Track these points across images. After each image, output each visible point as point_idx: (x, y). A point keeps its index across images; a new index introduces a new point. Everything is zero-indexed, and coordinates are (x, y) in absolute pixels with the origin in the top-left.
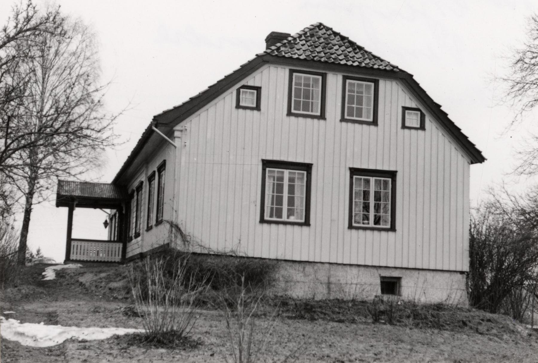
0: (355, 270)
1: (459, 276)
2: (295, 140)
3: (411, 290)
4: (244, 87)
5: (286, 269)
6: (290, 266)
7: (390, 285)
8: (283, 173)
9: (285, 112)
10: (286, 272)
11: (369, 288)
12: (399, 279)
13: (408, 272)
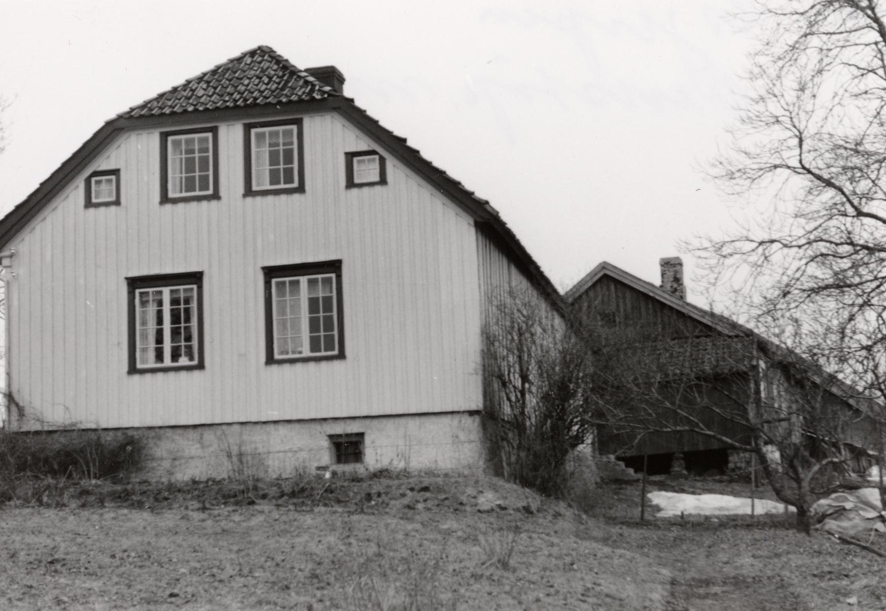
0: (282, 430)
1: (468, 421)
2: (169, 239)
3: (380, 452)
4: (96, 174)
5: (173, 441)
6: (180, 435)
7: (348, 447)
8: (161, 293)
9: (157, 197)
10: (173, 445)
11: (313, 453)
12: (361, 435)
13: (375, 422)
